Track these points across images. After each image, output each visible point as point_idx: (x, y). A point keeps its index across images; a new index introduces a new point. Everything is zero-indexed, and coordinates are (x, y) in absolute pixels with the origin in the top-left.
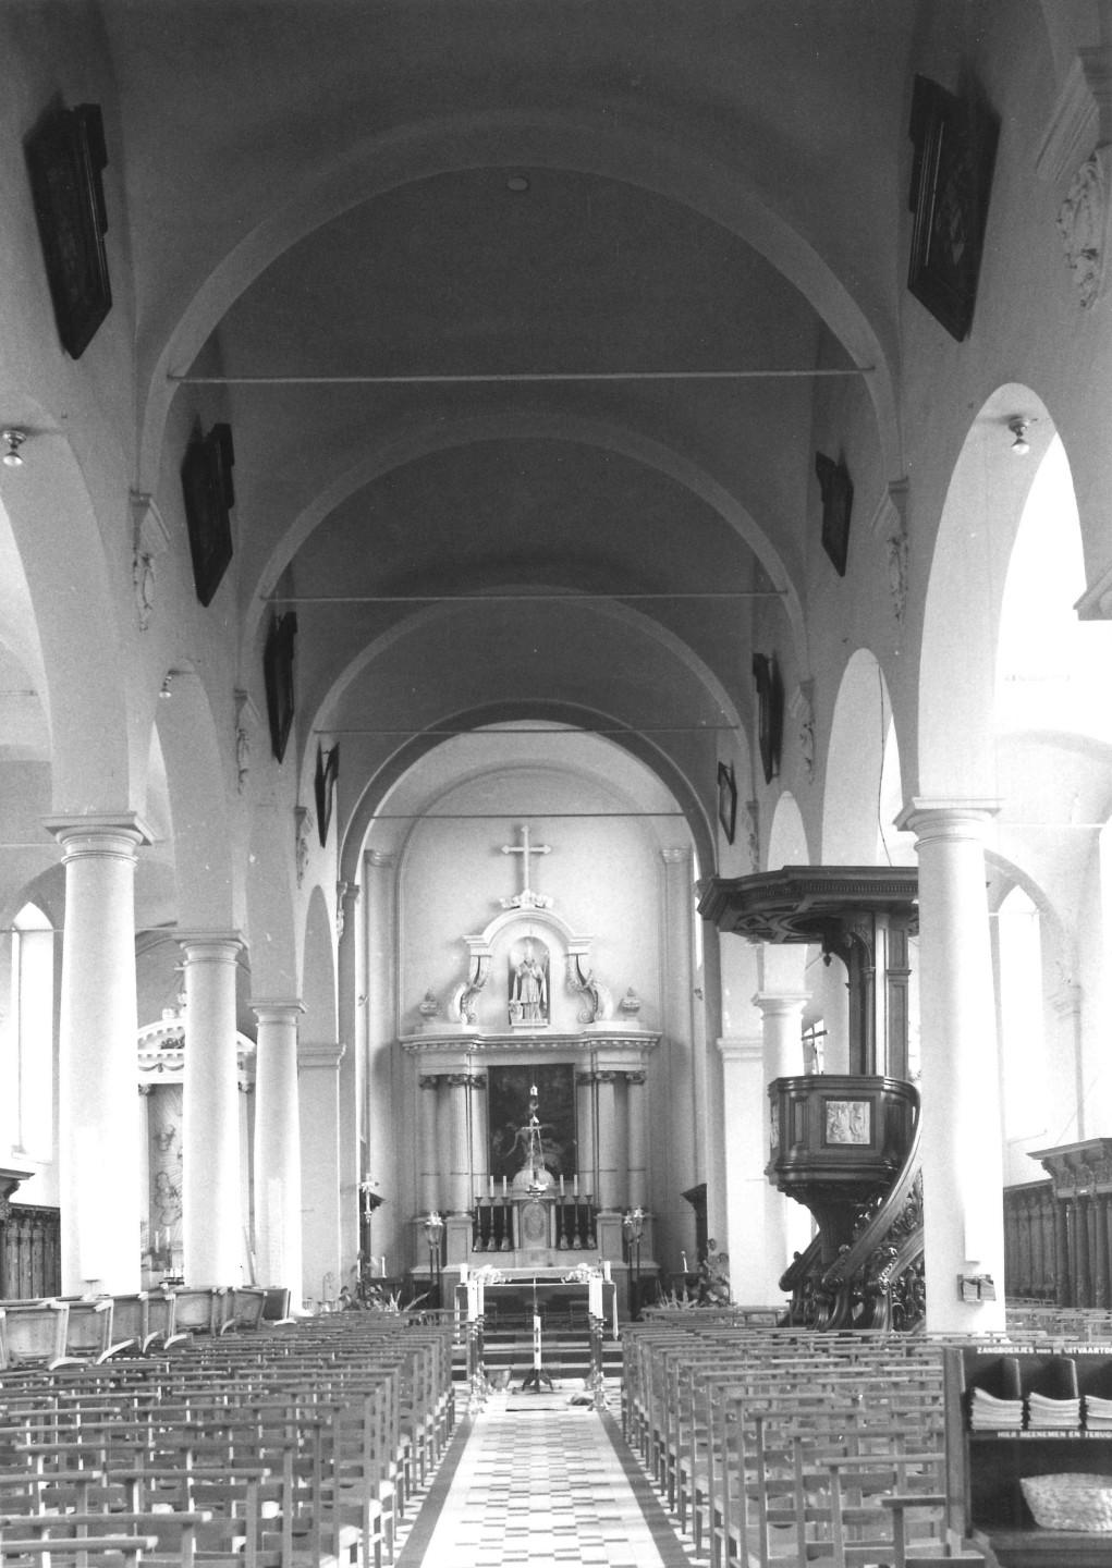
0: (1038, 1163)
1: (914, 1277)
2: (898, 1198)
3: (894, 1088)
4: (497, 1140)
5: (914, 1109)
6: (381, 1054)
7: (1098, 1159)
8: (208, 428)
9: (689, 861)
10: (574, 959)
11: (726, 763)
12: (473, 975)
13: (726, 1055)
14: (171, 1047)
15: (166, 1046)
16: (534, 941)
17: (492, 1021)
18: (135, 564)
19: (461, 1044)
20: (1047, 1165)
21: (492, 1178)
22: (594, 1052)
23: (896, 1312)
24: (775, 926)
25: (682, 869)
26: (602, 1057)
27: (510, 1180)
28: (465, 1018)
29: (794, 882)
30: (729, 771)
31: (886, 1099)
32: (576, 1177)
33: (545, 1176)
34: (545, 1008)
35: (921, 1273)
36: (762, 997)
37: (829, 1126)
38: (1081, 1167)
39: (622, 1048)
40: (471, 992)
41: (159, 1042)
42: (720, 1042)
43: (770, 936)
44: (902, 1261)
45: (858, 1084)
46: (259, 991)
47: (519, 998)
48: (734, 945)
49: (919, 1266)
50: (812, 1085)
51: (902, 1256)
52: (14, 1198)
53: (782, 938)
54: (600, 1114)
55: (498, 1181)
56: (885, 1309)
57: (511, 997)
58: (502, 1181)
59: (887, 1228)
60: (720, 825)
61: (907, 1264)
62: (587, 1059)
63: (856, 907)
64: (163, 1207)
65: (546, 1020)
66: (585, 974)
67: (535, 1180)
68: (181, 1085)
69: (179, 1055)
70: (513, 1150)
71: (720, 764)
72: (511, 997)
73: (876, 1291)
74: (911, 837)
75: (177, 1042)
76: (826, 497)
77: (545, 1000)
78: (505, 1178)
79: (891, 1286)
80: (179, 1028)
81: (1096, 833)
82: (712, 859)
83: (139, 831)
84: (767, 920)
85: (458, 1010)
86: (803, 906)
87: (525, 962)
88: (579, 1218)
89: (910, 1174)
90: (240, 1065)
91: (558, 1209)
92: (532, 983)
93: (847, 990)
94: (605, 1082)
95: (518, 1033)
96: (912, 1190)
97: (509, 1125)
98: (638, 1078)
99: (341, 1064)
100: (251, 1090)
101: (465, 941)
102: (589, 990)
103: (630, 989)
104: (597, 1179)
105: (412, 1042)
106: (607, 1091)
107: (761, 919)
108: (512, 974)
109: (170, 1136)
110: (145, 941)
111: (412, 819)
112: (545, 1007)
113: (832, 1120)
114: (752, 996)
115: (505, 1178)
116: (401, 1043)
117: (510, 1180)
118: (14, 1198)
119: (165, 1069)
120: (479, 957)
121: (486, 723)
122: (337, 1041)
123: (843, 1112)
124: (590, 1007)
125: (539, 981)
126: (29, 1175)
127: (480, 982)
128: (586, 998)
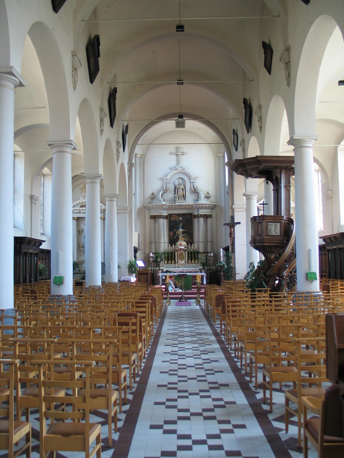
0: (322, 239)
1: (293, 273)
2: (288, 250)
3: (286, 219)
4: (171, 234)
5: (292, 225)
6: (139, 210)
7: (339, 238)
8: (93, 36)
9: (224, 156)
10: (192, 184)
11: (235, 129)
12: (165, 188)
13: (235, 210)
14: (83, 207)
15: (81, 207)
16: (181, 178)
17: (170, 201)
18: (72, 71)
19: (162, 207)
20: (324, 240)
21: (170, 245)
22: (198, 209)
23: (288, 283)
24: (253, 173)
25: (222, 158)
26: (200, 211)
27: (175, 245)
28: (162, 200)
29: (257, 160)
30: (236, 131)
31: (284, 222)
32: (193, 244)
33: (184, 243)
34: (184, 197)
35: (295, 272)
36: (246, 194)
37: (268, 230)
38: (334, 240)
39: (206, 208)
40: (165, 192)
41: (79, 205)
42: (233, 206)
43: (252, 176)
44: (290, 269)
45: (277, 217)
46: (106, 191)
47: (177, 194)
48: (239, 178)
49: (294, 270)
50: (263, 218)
51: (290, 268)
52: (41, 247)
53: (254, 177)
54: (199, 226)
55: (171, 245)
56: (285, 282)
57: (175, 194)
58: (172, 245)
59: (285, 259)
60: (233, 146)
61: (291, 269)
62: (196, 211)
63: (277, 167)
64: (80, 251)
65: (185, 200)
66: (195, 188)
67: (182, 244)
68: (85, 217)
69: (85, 209)
70: (176, 237)
71: (234, 130)
72: (175, 194)
73: (282, 277)
74: (292, 147)
75: (84, 206)
76: (265, 53)
77: (184, 195)
78: (173, 245)
79: (287, 276)
80: (85, 202)
81: (336, 150)
82: (231, 156)
83: (73, 145)
84: (251, 171)
85: (161, 198)
86: (261, 167)
87: (179, 184)
88: (194, 255)
89: (291, 244)
90: (101, 212)
91: (188, 252)
92: (181, 190)
93: (273, 191)
94: (201, 217)
95: (177, 204)
96: (292, 248)
97: (175, 230)
98: (210, 216)
99: (129, 212)
100: (104, 219)
101: (162, 178)
102: (197, 192)
103: (208, 192)
104: (199, 245)
105: (148, 206)
106: (202, 220)
107: (249, 171)
108: (175, 187)
109: (82, 231)
110: (75, 178)
111: (148, 145)
112: (184, 197)
113: (269, 228)
114: (243, 194)
115: (173, 245)
116: (145, 207)
117: (175, 245)
118: (41, 247)
119: (81, 213)
120: (166, 183)
121: (170, 118)
122: (128, 206)
123: (272, 226)
124: (197, 197)
125: (183, 189)
126: (44, 241)
127: (166, 190)
128: (196, 194)
